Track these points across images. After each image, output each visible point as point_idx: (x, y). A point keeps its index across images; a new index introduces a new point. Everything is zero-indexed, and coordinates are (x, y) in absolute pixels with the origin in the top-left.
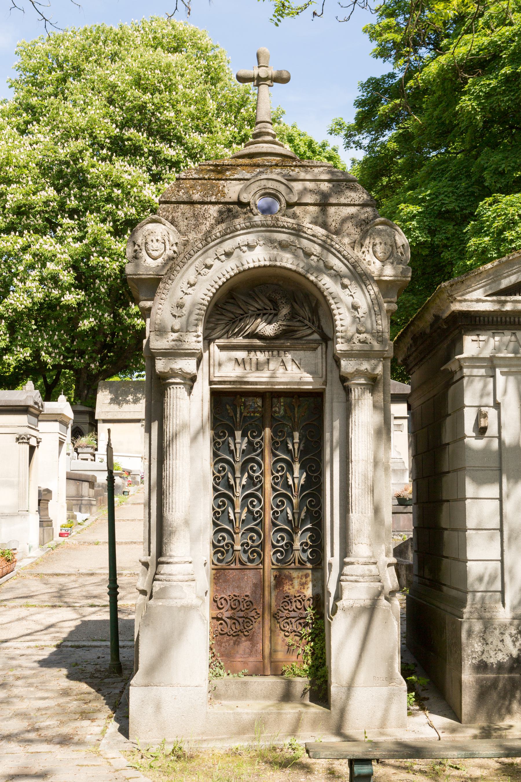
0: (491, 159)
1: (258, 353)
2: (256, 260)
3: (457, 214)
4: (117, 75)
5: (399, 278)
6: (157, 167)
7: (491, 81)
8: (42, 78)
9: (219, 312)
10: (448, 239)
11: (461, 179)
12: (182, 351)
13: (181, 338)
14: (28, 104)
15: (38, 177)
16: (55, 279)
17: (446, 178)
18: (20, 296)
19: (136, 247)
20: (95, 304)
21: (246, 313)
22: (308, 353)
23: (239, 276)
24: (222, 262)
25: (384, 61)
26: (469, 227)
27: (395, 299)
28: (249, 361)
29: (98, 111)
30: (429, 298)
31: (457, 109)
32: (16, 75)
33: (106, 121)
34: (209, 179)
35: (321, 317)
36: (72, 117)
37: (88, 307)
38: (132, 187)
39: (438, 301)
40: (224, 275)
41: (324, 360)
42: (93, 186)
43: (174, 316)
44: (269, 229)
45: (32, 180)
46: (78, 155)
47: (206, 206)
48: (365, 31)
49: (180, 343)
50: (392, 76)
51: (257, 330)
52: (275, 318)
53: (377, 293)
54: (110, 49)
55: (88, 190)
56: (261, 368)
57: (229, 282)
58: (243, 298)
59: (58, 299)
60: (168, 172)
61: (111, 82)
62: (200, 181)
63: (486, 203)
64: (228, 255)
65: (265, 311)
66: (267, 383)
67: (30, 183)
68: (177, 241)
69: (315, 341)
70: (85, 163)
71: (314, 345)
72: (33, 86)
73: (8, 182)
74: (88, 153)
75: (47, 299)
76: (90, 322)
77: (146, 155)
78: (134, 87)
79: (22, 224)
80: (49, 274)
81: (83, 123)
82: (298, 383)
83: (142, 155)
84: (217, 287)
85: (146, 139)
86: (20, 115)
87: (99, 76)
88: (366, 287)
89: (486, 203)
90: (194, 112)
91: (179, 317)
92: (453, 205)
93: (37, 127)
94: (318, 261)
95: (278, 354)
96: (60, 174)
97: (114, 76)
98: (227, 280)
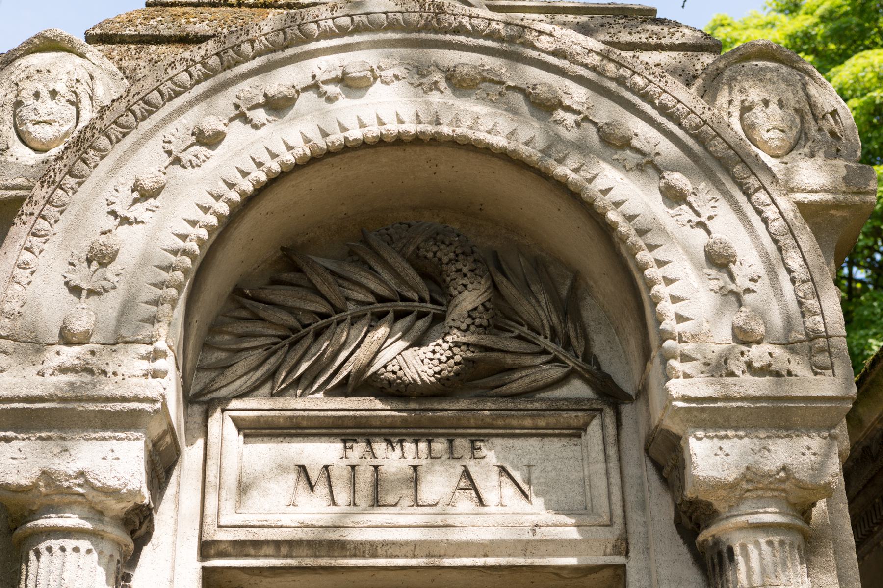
1: (380, 447)
5: (841, 197)
9: (244, 314)
12: (91, 407)
13: (93, 360)
21: (338, 311)
22: (555, 446)
24: (256, 127)
28: (346, 473)
35: (592, 326)
41: (613, 464)
43: (76, 290)
44: (414, 35)
49: (87, 378)
51: (377, 366)
52: (438, 328)
56: (391, 499)
64: (278, 106)
65: (401, 306)
66: (413, 549)
69: (576, 404)
71: (574, 418)
82: (526, 547)
91: (92, 292)
94: (578, 124)
95: (451, 449)
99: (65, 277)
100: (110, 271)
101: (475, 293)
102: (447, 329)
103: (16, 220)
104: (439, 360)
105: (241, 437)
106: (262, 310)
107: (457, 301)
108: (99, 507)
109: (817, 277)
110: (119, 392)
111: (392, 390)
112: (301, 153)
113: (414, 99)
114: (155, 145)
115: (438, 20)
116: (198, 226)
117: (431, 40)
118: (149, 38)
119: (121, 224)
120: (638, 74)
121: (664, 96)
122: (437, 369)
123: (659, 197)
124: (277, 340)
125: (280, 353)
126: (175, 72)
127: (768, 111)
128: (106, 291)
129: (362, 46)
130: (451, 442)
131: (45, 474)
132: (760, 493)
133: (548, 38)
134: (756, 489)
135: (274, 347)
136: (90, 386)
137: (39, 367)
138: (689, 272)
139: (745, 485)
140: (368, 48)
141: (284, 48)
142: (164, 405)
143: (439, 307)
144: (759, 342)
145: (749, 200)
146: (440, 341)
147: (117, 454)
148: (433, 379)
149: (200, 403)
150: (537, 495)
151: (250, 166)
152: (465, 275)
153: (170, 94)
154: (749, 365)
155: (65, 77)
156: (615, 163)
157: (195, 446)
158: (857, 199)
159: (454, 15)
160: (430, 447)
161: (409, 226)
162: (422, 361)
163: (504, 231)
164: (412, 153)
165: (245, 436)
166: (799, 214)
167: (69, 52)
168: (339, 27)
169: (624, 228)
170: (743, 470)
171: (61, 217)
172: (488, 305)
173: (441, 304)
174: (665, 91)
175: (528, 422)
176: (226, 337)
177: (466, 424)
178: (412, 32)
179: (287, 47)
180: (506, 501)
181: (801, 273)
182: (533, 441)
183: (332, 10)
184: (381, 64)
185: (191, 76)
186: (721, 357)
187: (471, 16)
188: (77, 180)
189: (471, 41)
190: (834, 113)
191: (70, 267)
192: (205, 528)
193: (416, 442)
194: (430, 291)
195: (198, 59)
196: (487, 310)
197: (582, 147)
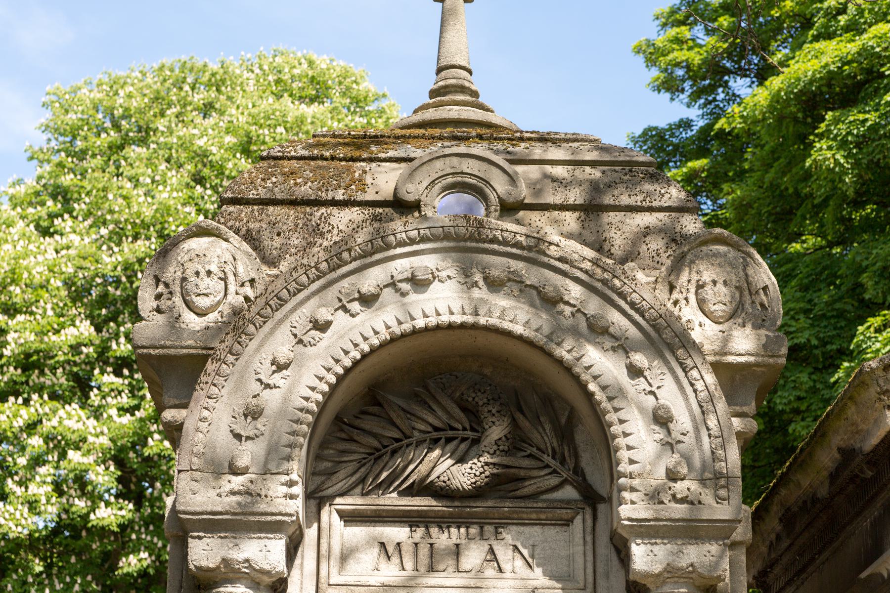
0: (874, 252)
1: (434, 531)
2: (430, 311)
3: (816, 352)
4: (209, 137)
7: (867, 116)
8: (85, 144)
9: (343, 436)
10: (799, 399)
11: (820, 290)
14: (59, 187)
16: (81, 481)
17: (792, 288)
18: (16, 510)
19: (161, 288)
20: (151, 528)
21: (407, 437)
22: (552, 532)
23: (394, 349)
24: (353, 316)
25: (672, 99)
26: (840, 373)
27: (751, 408)
29: (175, 194)
30: (829, 408)
31: (807, 164)
32: (40, 140)
33: (187, 209)
34: (333, 158)
37: (138, 533)
39: (851, 411)
40: (356, 345)
41: (589, 547)
43: (238, 437)
45: (53, 309)
46: (137, 267)
47: (323, 210)
48: (638, 50)
49: (249, 499)
50: (686, 124)
52: (475, 448)
53: (712, 388)
54: (199, 98)
56: (441, 568)
58: (401, 402)
59: (85, 517)
61: (200, 147)
62: (312, 163)
63: (869, 327)
65: (450, 433)
67: (50, 313)
68: (253, 275)
71: (565, 513)
73: (11, 311)
75: (64, 516)
76: (140, 560)
78: (238, 155)
79: (31, 383)
80: (71, 471)
81: (148, 213)
84: (340, 371)
86: (43, 204)
87: (179, 138)
88: (686, 373)
89: (869, 327)
91: (248, 438)
92: (806, 334)
93: (70, 222)
94: (573, 315)
96: (104, 300)
97: (205, 139)
100: (259, 423)
101: (500, 428)
102: (481, 453)
103: (197, 387)
105: (342, 523)
107: (487, 434)
108: (257, 580)
109: (725, 434)
110: (269, 510)
111: (443, 493)
113: (461, 295)
114: (285, 329)
119: (265, 388)
120: (617, 278)
121: (634, 295)
122: (473, 481)
123: (625, 371)
124: (366, 456)
125: (368, 465)
126: (298, 275)
127: (716, 289)
128: (257, 437)
130: (482, 528)
131: (224, 560)
132: (676, 579)
133: (556, 248)
134: (673, 577)
135: (364, 461)
137: (218, 491)
138: (640, 428)
139: (666, 575)
140: (430, 253)
141: (372, 254)
142: (298, 517)
143: (476, 434)
144: (682, 479)
145: (686, 375)
146: (475, 461)
147: (268, 548)
148: (470, 487)
149: (315, 498)
150: (538, 566)
152: (494, 415)
154: (674, 496)
155: (216, 260)
156: (596, 344)
157: (312, 528)
158: (771, 360)
160: (467, 531)
164: (457, 332)
165: (345, 521)
166: (718, 387)
167: (217, 237)
169: (599, 396)
170: (664, 566)
172: (509, 436)
173: (477, 431)
174: (635, 291)
175: (534, 516)
176: (331, 451)
177: (492, 516)
178: (460, 241)
179: (374, 253)
180: (517, 570)
181: (715, 431)
182: (536, 528)
185: (308, 277)
186: (656, 490)
187: (502, 230)
189: (502, 249)
190: (765, 289)
192: (320, 586)
193: (459, 528)
194: (470, 422)
195: (313, 264)
196: (508, 439)
197: (575, 332)
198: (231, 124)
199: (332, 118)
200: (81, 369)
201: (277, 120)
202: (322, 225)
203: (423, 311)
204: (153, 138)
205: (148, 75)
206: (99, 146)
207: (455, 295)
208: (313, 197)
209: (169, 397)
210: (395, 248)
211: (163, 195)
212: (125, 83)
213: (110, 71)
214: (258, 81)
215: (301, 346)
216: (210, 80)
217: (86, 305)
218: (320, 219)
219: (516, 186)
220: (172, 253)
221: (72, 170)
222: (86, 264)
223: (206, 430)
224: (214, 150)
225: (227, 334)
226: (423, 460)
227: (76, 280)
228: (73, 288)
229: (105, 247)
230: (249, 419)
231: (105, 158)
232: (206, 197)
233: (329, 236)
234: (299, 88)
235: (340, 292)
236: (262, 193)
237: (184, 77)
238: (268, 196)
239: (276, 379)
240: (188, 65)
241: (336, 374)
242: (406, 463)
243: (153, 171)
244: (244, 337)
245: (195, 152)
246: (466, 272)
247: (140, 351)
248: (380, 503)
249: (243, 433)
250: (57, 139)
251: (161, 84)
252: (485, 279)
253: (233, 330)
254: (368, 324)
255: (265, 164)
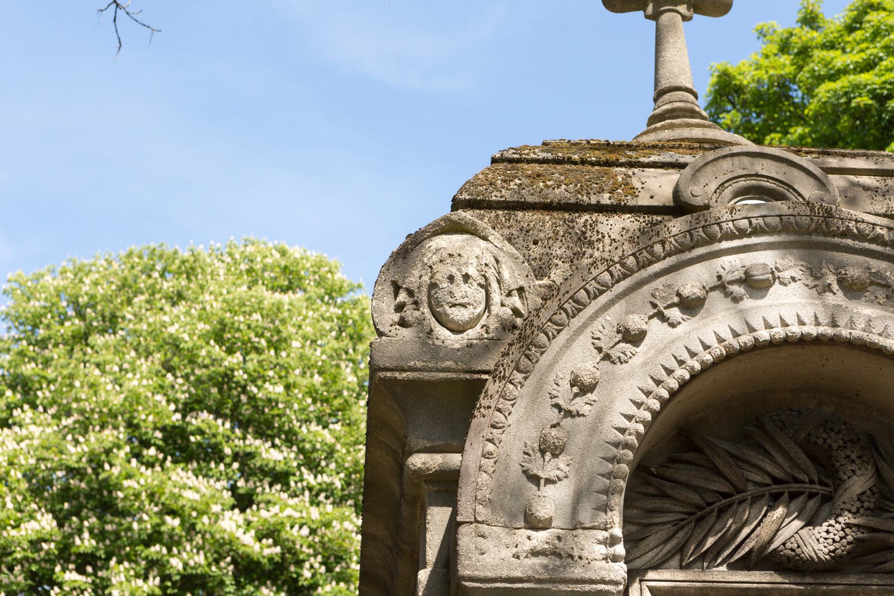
2: (774, 320)
4: (178, 323)
6: (247, 481)
8: (47, 332)
9: (651, 490)
15: (25, 499)
19: (402, 297)
21: (739, 492)
24: (673, 325)
29: (145, 382)
36: (96, 393)
38: (201, 513)
42: (124, 513)
46: (103, 457)
54: (168, 285)
55: (117, 520)
57: (660, 418)
58: (726, 446)
60: (267, 490)
61: (171, 335)
65: (795, 487)
68: (522, 282)
70: (116, 471)
72: (29, 344)
74: (122, 454)
77: (228, 460)
78: (212, 342)
81: (117, 401)
83: (221, 459)
85: (229, 433)
90: (318, 386)
97: (177, 326)
98: (694, 377)
99: (523, 466)
101: (863, 478)
102: (839, 511)
103: (476, 413)
104: (833, 539)
106: (668, 488)
107: (847, 485)
110: (587, 575)
112: (719, 353)
113: (811, 301)
114: (584, 342)
115: (827, 224)
116: (633, 421)
117: (821, 243)
118: (515, 205)
119: (565, 417)
122: (832, 548)
124: (684, 516)
125: (687, 528)
126: (598, 271)
128: (560, 480)
129: (759, 247)
135: (682, 523)
136: (561, 569)
137: (514, 550)
140: (765, 249)
143: (826, 489)
146: (832, 522)
148: (828, 557)
151: (672, 364)
152: (853, 461)
153: (595, 293)
155: (474, 261)
159: (842, 219)
161: (800, 413)
162: (818, 540)
163: (875, 414)
167: (472, 234)
168: (739, 229)
171: (513, 410)
176: (635, 511)
178: (803, 234)
179: (693, 247)
183: (731, 213)
184: (778, 265)
185: (612, 275)
187: (856, 221)
188: (524, 375)
189: (858, 244)
191: (526, 456)
194: (818, 473)
195: (616, 259)
196: (873, 494)
198: (203, 312)
199: (307, 308)
200: (40, 567)
201: (253, 307)
202: (589, 234)
203: (764, 320)
204: (122, 325)
205: (113, 263)
206: (62, 335)
207: (804, 301)
208: (573, 201)
209: (417, 437)
210: (720, 241)
211: (132, 382)
212: (90, 271)
213: (75, 258)
214: (229, 270)
215: (607, 363)
216: (180, 267)
217: (46, 500)
218: (585, 226)
219: (827, 191)
220: (414, 254)
221: (33, 359)
222: (46, 454)
223: (492, 470)
224: (186, 337)
225: (510, 345)
226: (761, 521)
227: (38, 472)
228: (34, 481)
229: (69, 437)
230: (548, 456)
231: (68, 348)
232: (177, 386)
233: (600, 246)
234: (271, 278)
235: (653, 295)
236: (507, 195)
237: (159, 263)
238: (515, 198)
239: (579, 405)
240: (157, 253)
241: (660, 398)
242: (739, 525)
243: (120, 359)
244: (534, 349)
245: (164, 340)
246: (814, 273)
247: (382, 374)
248: (707, 579)
249: (541, 474)
250: (17, 328)
251: (129, 271)
252: (840, 282)
253: (520, 339)
254: (694, 336)
255: (501, 166)
